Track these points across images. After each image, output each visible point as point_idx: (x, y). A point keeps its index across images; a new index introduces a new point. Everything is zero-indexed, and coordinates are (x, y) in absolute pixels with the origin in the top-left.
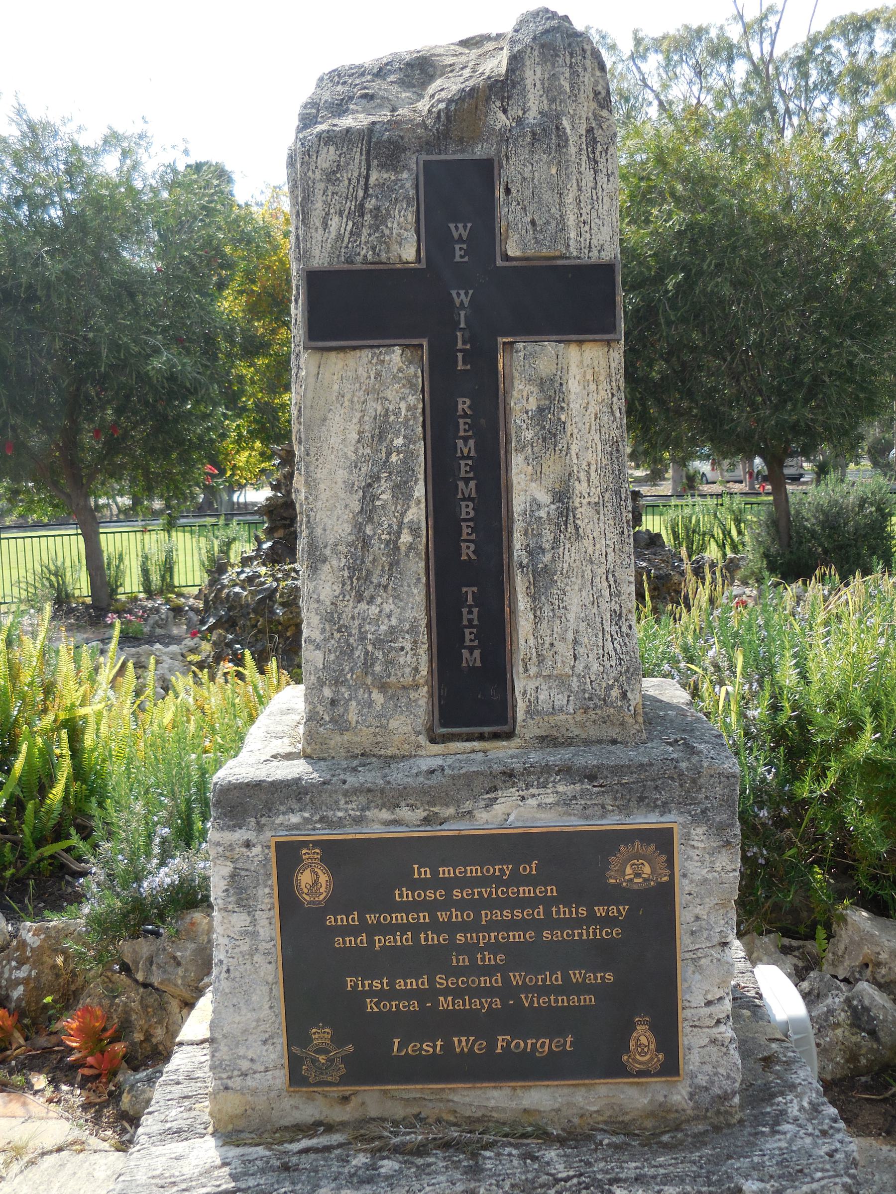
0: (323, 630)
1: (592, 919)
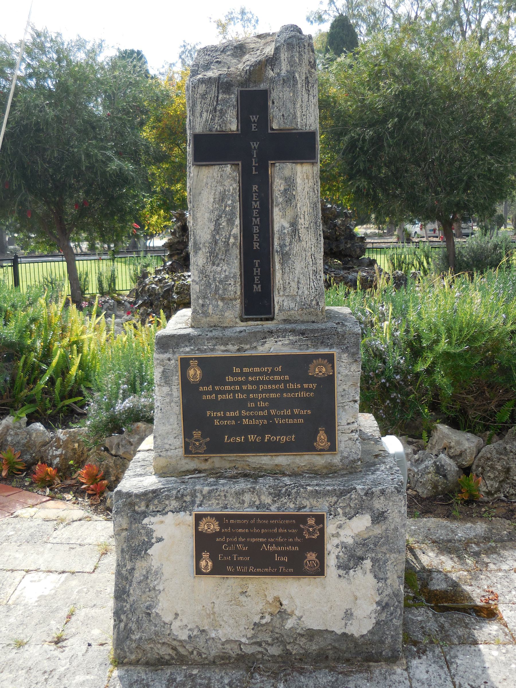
0: (199, 277)
1: (302, 389)
